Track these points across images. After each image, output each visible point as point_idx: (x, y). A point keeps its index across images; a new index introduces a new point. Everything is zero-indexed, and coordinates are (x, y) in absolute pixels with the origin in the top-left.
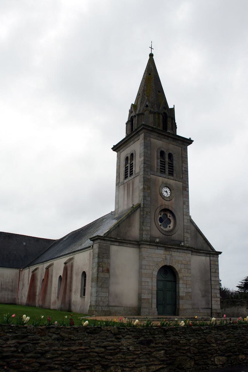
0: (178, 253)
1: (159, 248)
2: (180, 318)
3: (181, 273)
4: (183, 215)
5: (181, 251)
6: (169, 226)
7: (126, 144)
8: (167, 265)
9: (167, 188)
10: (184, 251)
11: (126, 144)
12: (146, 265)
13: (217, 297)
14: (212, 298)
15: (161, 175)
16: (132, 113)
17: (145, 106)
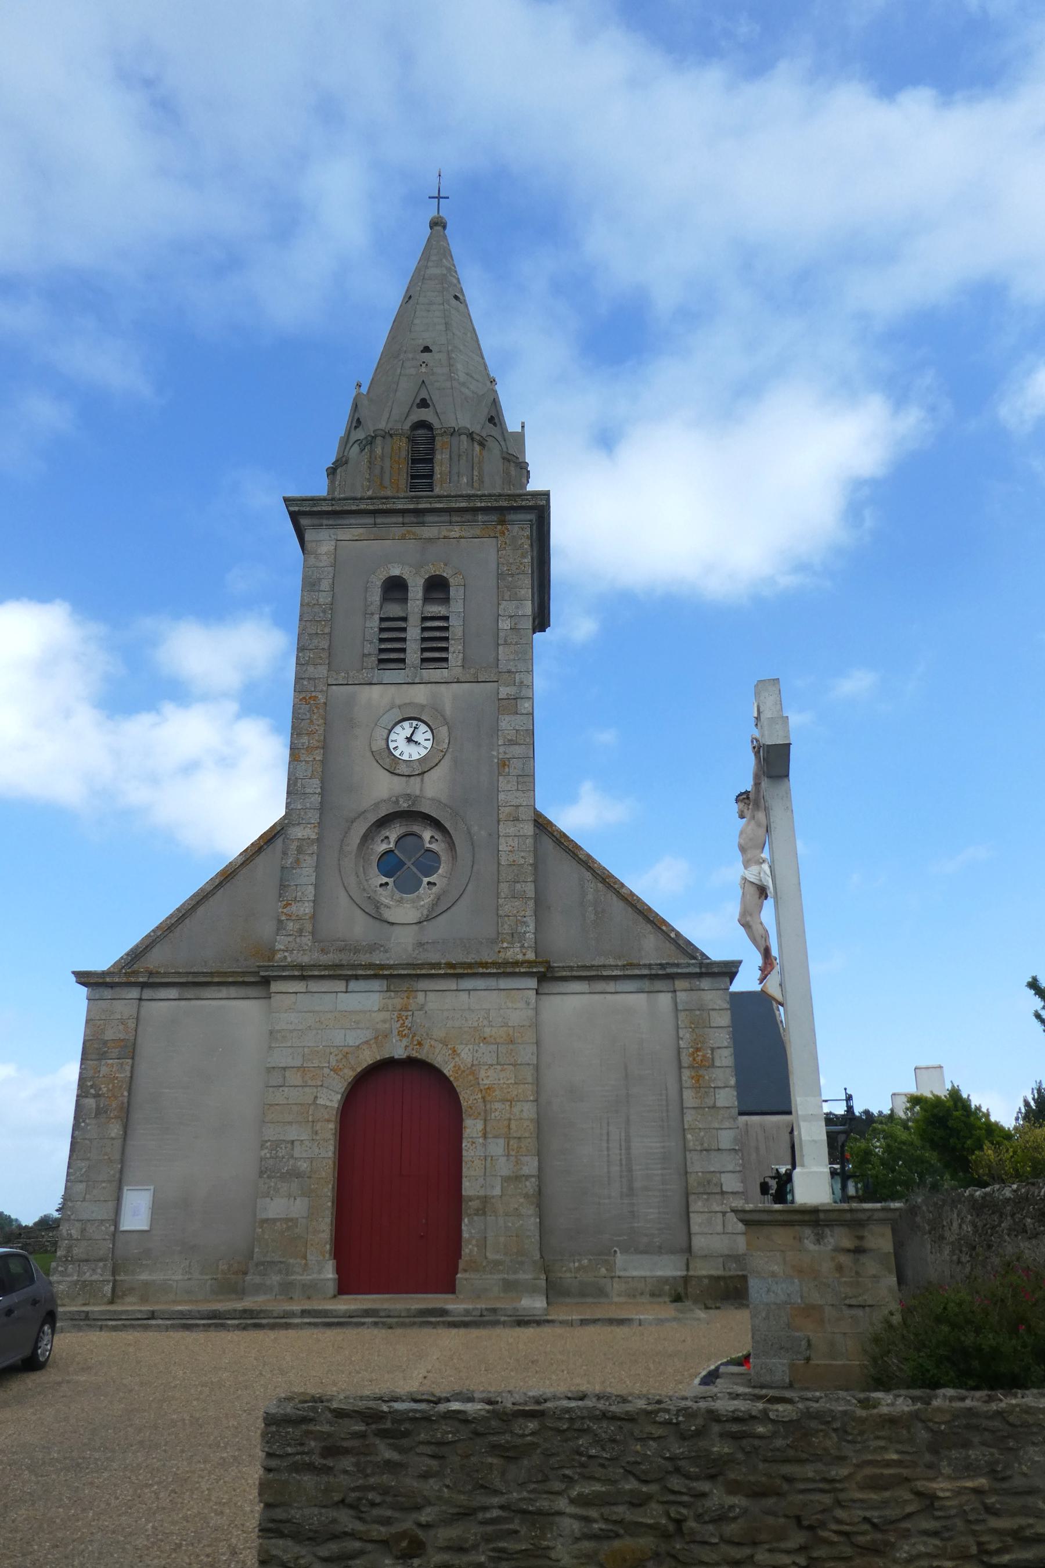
0: (464, 996)
1: (353, 985)
2: (83, 1316)
3: (713, 1066)
4: (499, 821)
5: (480, 983)
6: (387, 884)
7: (331, 522)
8: (396, 1057)
9: (393, 736)
10: (492, 983)
11: (331, 522)
12: (284, 1069)
13: (723, 1193)
14: (692, 1198)
15: (389, 676)
16: (356, 427)
17: (418, 401)
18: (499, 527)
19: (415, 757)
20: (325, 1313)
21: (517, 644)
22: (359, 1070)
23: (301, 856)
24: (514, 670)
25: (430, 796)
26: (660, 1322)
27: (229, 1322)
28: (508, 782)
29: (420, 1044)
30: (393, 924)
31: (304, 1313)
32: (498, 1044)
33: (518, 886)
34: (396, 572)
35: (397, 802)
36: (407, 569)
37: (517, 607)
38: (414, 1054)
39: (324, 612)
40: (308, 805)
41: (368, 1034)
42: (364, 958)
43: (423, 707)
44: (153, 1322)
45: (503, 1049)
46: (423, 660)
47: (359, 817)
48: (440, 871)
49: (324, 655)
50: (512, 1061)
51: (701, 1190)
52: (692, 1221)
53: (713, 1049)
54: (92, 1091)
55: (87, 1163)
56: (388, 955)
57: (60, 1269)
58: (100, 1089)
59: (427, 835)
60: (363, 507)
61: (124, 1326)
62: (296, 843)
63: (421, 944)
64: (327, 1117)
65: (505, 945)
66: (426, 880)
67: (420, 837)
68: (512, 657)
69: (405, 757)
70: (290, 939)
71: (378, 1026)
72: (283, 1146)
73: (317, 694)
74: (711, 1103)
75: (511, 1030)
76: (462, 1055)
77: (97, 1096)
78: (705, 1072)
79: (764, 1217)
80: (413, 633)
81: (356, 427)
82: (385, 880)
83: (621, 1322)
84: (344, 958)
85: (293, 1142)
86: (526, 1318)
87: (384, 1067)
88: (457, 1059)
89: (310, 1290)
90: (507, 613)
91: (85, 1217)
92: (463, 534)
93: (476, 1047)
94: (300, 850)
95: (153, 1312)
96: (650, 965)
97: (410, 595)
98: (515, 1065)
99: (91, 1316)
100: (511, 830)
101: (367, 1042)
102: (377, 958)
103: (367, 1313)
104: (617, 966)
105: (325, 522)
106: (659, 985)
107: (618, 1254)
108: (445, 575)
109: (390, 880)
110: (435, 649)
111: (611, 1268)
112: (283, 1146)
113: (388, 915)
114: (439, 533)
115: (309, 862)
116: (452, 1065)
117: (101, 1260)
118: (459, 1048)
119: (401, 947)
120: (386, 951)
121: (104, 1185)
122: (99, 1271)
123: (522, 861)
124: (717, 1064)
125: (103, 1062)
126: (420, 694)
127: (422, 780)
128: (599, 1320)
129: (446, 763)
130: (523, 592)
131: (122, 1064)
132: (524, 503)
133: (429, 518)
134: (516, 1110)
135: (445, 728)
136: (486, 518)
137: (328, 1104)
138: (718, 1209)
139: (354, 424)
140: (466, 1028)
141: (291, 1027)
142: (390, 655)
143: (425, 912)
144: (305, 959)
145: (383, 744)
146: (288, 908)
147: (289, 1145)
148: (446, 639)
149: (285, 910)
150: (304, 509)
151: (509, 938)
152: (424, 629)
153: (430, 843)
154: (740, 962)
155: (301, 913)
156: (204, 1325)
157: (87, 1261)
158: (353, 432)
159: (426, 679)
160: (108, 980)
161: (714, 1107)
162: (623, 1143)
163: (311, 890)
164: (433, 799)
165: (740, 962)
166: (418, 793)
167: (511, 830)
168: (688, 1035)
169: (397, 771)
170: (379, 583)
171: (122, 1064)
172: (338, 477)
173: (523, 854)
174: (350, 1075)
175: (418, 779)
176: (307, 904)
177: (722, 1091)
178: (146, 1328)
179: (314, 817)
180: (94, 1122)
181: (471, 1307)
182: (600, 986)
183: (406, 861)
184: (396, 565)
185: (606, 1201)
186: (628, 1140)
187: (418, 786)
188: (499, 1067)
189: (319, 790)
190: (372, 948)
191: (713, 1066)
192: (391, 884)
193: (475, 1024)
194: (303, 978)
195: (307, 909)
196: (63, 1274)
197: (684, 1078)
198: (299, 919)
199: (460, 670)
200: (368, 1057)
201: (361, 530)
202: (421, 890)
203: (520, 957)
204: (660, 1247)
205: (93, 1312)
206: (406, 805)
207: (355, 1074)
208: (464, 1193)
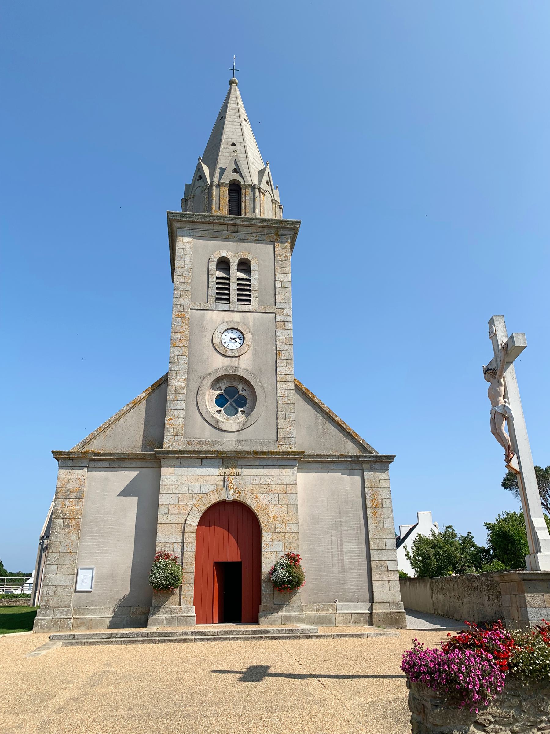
6: (220, 411)
11: (190, 226)
13: (388, 571)
16: (198, 180)
18: (275, 236)
19: (235, 347)
20: (204, 633)
21: (284, 295)
22: (208, 506)
23: (177, 395)
24: (283, 307)
25: (242, 368)
26: (377, 635)
27: (155, 639)
28: (282, 363)
29: (239, 493)
30: (224, 431)
31: (193, 633)
32: (278, 493)
33: (287, 414)
34: (224, 255)
35: (226, 369)
36: (230, 253)
37: (285, 277)
38: (237, 498)
39: (188, 271)
40: (181, 369)
41: (213, 488)
42: (210, 448)
43: (239, 323)
44: (112, 640)
45: (281, 496)
46: (239, 300)
47: (207, 376)
48: (247, 405)
49: (188, 293)
50: (286, 503)
51: (378, 570)
52: (374, 585)
53: (382, 499)
54: (61, 515)
55: (58, 554)
56: (222, 447)
57: (42, 612)
58: (66, 514)
59: (240, 387)
60: (207, 220)
61: (98, 642)
62: (174, 388)
63: (239, 442)
64: (191, 530)
65: (281, 443)
66: (240, 409)
67: (237, 388)
68: (283, 301)
69: (230, 347)
70: (172, 437)
71: (217, 483)
72: (168, 545)
73: (185, 313)
74: (382, 526)
75: (285, 486)
76: (261, 499)
77: (63, 518)
78: (379, 511)
79: (533, 577)
80: (234, 286)
81: (198, 180)
82: (219, 408)
83: (358, 636)
84: (201, 448)
85: (173, 543)
86: (311, 634)
87: (221, 504)
88: (258, 501)
89: (183, 621)
90: (279, 280)
91: (57, 584)
92: (257, 238)
93: (268, 495)
94: (176, 392)
95: (111, 634)
96: (352, 456)
97: (231, 267)
98: (287, 504)
99: (76, 637)
100: (284, 386)
101: (212, 491)
102: (218, 448)
103: (226, 633)
104: (335, 456)
105: (187, 226)
106: (355, 466)
107: (337, 602)
108: (248, 258)
109: (222, 409)
110: (245, 295)
111: (335, 609)
112: (168, 545)
113: (222, 427)
114: (245, 237)
115: (182, 397)
116: (256, 504)
117: (65, 607)
118: (259, 495)
119: (228, 443)
120: (221, 445)
121: (67, 566)
122: (65, 613)
123: (289, 402)
124: (384, 506)
125: (68, 500)
126: (237, 317)
127: (239, 359)
128: (347, 635)
129: (250, 352)
130: (287, 269)
131: (78, 501)
132: (288, 226)
133: (241, 229)
134: (288, 528)
135: (250, 334)
136: (269, 232)
137: (192, 523)
138: (386, 579)
139: (198, 178)
140: (254, 486)
141: (172, 483)
142: (223, 296)
143: (241, 425)
144: (180, 448)
145: (219, 340)
146: (171, 421)
147: (171, 545)
148: (239, 290)
149: (169, 422)
150: (176, 218)
151: (283, 440)
152: (239, 284)
153: (221, 390)
154: (395, 456)
155: (177, 424)
156: (142, 641)
157: (58, 607)
158: (197, 182)
159: (240, 309)
160: (71, 456)
161: (383, 528)
162: (339, 546)
163: (182, 413)
164: (244, 369)
165: (395, 456)
166: (237, 365)
167: (284, 386)
168: (370, 492)
169: (226, 354)
170: (216, 260)
171: (78, 501)
172: (189, 204)
173: (289, 398)
174: (203, 508)
175: (237, 359)
176: (180, 419)
177: (387, 520)
178: (109, 643)
179: (185, 375)
180: (62, 532)
181: (280, 629)
182: (327, 465)
183: (233, 400)
184: (224, 251)
185: (331, 575)
186: (341, 544)
187: (237, 362)
188: (279, 505)
189: (187, 362)
190: (214, 443)
191: (382, 507)
192: (223, 411)
193: (267, 483)
194: (178, 458)
195: (181, 422)
196: (43, 615)
197: (368, 513)
198: (176, 427)
199: (257, 306)
200: (213, 499)
201: (206, 232)
202: (238, 414)
203: (289, 450)
204: (358, 598)
205: (77, 635)
206: (231, 371)
207: (206, 508)
208: (263, 570)
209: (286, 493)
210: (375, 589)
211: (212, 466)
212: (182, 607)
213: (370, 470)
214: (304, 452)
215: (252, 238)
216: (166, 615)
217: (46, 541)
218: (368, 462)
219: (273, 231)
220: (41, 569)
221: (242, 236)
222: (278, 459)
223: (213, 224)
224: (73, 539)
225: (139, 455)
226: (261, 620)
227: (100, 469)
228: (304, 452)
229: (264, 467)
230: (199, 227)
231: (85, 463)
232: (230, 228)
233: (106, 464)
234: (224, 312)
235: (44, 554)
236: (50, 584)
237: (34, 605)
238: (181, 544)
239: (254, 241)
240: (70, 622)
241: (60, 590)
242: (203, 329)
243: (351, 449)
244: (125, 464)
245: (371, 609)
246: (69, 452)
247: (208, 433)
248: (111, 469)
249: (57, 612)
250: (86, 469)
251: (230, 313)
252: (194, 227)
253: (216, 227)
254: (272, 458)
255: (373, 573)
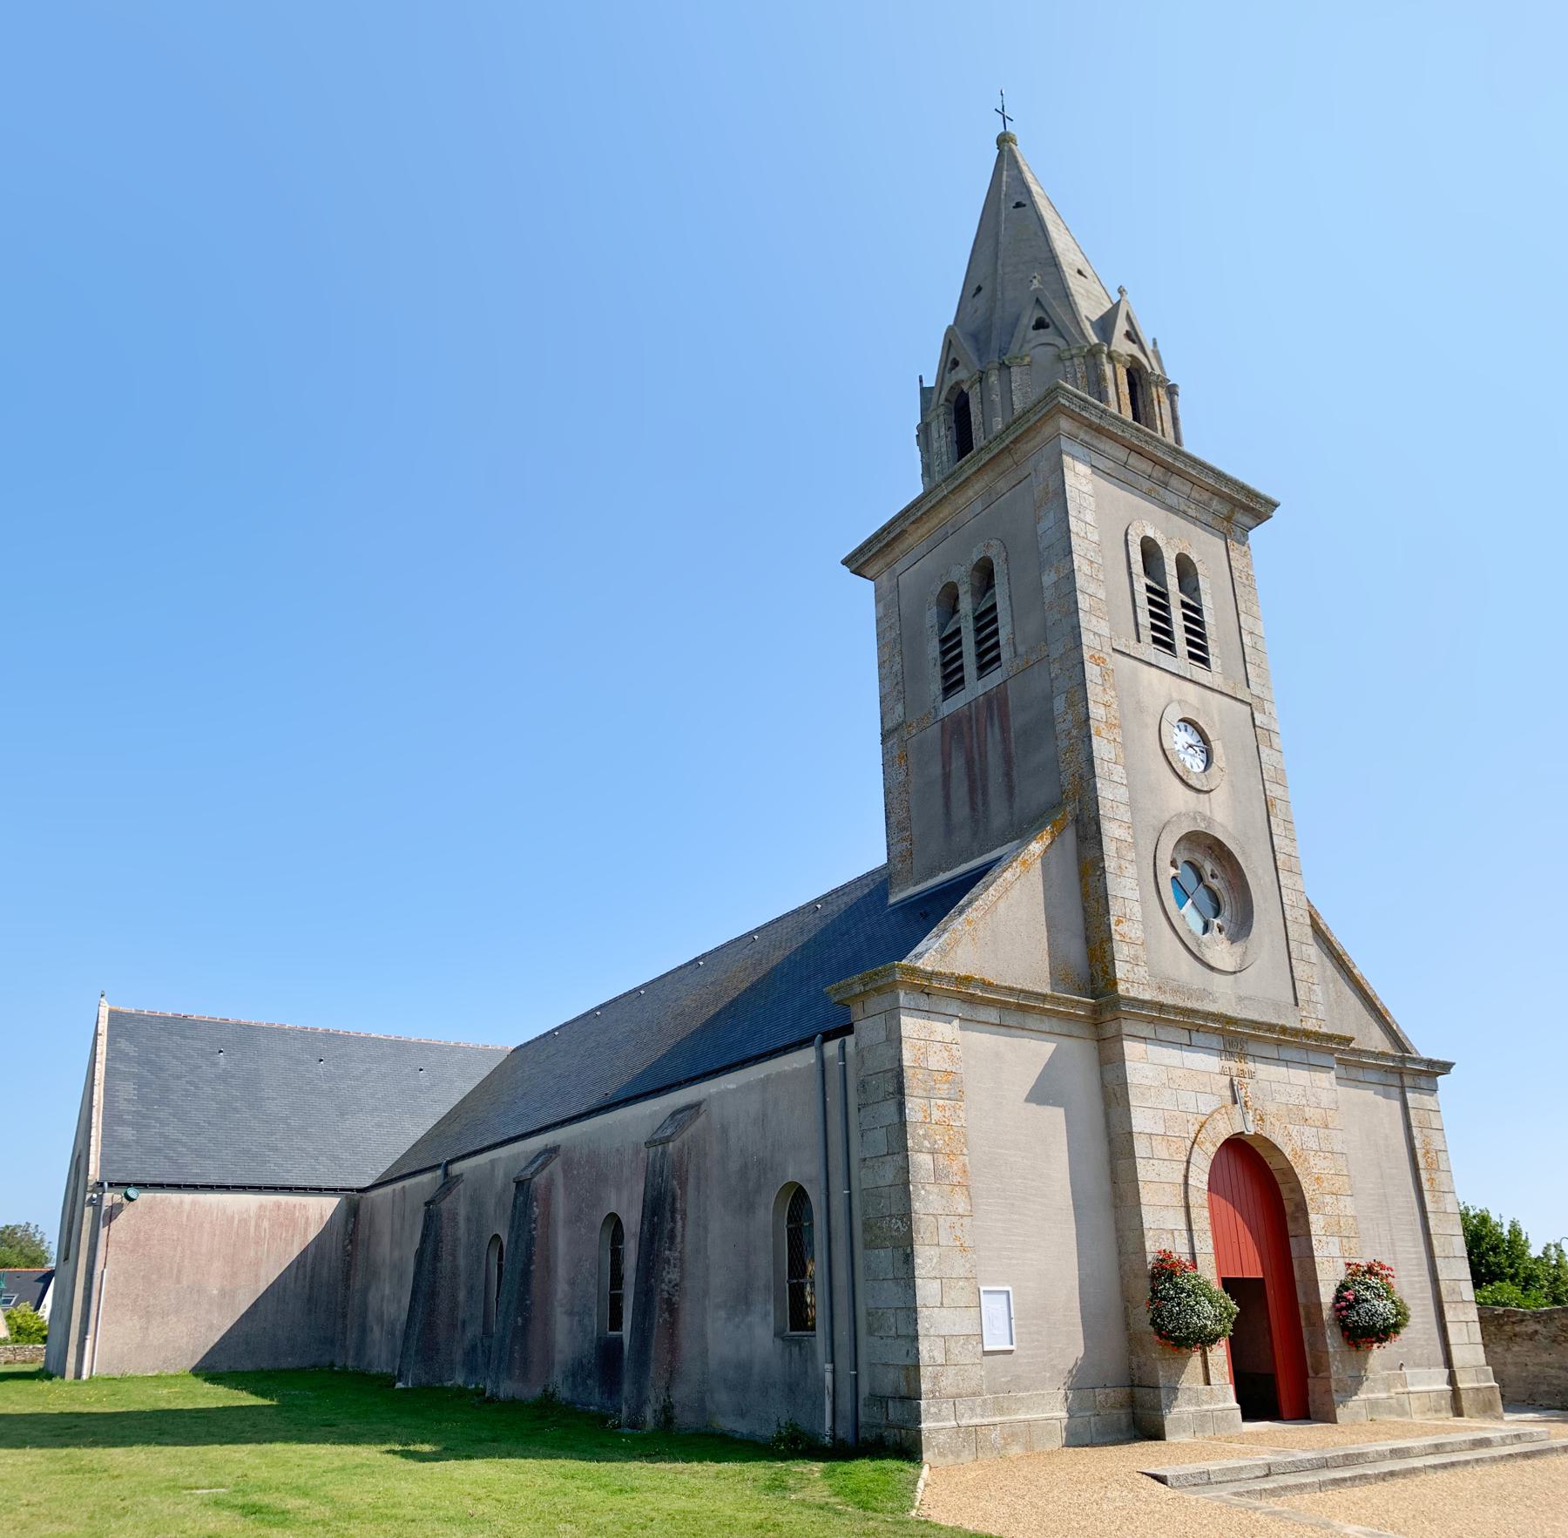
11: (1087, 438)
30: (1212, 968)
77: (933, 1152)
85: (1172, 1231)
122: (978, 1410)
133: (1175, 482)
182: (1360, 1074)
209: (1327, 1127)
210: (1452, 1340)
211: (1207, 1049)
212: (1205, 1389)
213: (1415, 1088)
214: (1351, 1040)
215: (1191, 512)
216: (1192, 1409)
217: (107, 1196)
218: (1408, 1072)
219: (1224, 509)
220: (97, 1272)
221: (1172, 499)
222: (1307, 1048)
223: (1132, 449)
224: (960, 1211)
225: (1043, 997)
226: (1339, 1411)
227: (979, 1026)
228: (1351, 1040)
229: (1287, 1063)
230: (1101, 446)
231: (953, 1007)
232: (1158, 472)
233: (992, 1015)
234: (1168, 676)
235: (103, 1232)
236: (932, 1332)
237: (78, 1375)
238: (1185, 1234)
239: (1195, 520)
240: (994, 1435)
241: (955, 1348)
242: (1140, 708)
243: (1376, 1041)
244: (1032, 1021)
245: (1452, 1380)
246: (932, 973)
247: (1185, 969)
248: (1003, 1030)
249: (960, 1408)
250: (956, 1022)
251: (1179, 680)
252: (1095, 442)
253: (1134, 460)
254: (1301, 1046)
255: (1446, 1306)
